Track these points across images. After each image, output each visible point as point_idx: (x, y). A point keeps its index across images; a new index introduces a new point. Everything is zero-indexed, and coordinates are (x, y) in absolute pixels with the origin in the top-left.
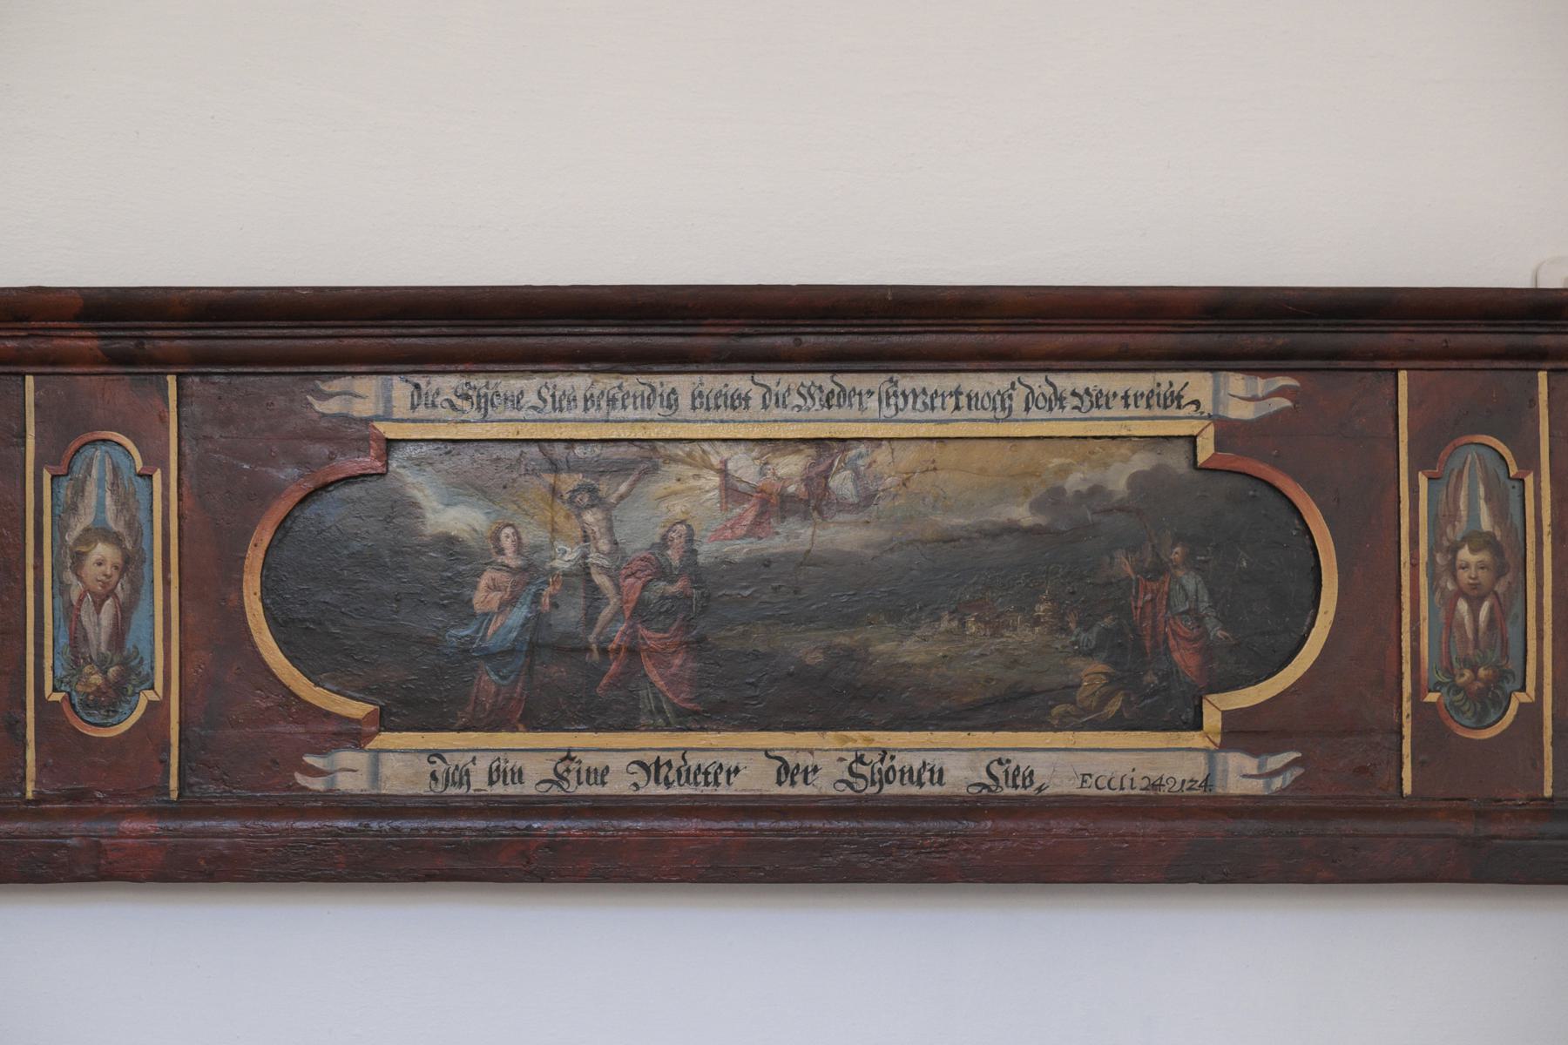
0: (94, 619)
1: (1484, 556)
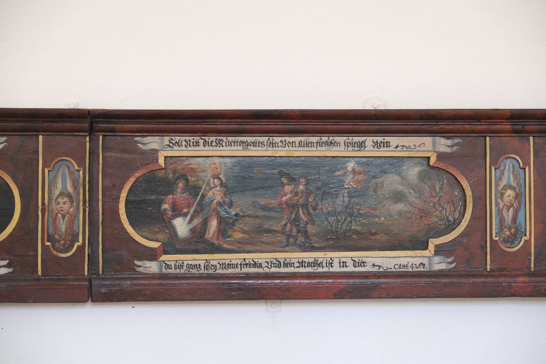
0: (507, 214)
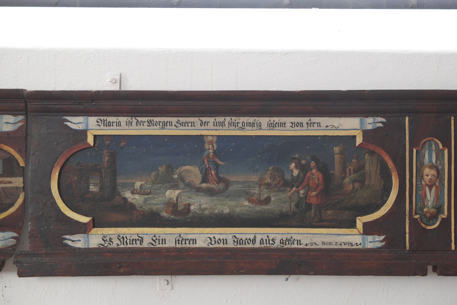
1: (433, 172)
